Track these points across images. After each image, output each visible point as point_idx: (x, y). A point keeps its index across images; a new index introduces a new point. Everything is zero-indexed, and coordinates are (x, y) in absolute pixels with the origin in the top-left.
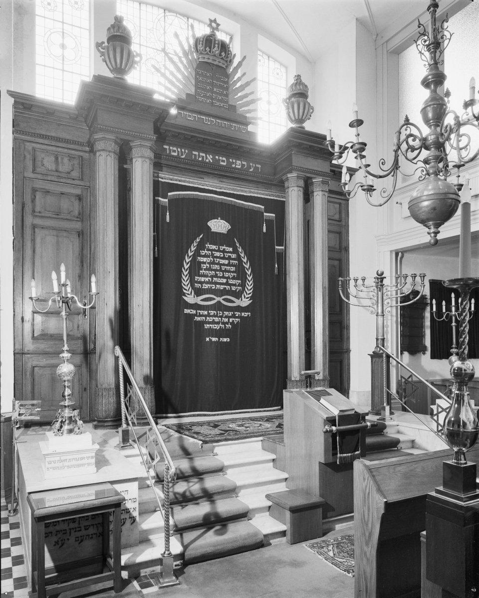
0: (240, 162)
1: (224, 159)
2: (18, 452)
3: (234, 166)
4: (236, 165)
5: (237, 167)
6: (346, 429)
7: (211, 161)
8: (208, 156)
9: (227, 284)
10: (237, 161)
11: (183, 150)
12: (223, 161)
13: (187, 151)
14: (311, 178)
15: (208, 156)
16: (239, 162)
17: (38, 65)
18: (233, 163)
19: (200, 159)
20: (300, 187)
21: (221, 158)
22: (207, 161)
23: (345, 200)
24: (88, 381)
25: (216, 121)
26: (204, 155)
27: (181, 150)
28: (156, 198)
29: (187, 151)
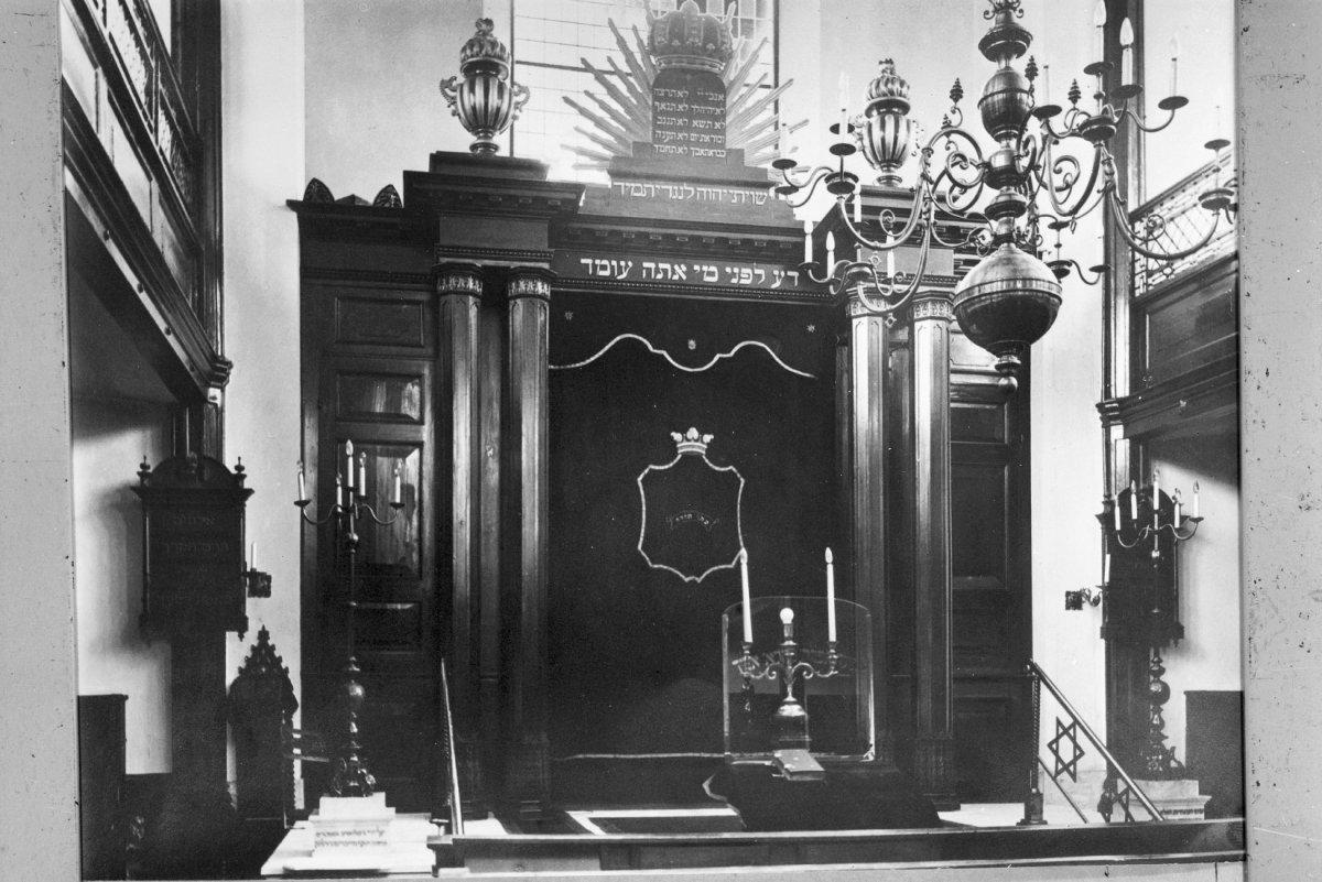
0: (749, 271)
3: (734, 281)
4: (740, 278)
5: (742, 281)
7: (684, 277)
10: (744, 270)
15: (676, 267)
19: (660, 276)
22: (676, 277)
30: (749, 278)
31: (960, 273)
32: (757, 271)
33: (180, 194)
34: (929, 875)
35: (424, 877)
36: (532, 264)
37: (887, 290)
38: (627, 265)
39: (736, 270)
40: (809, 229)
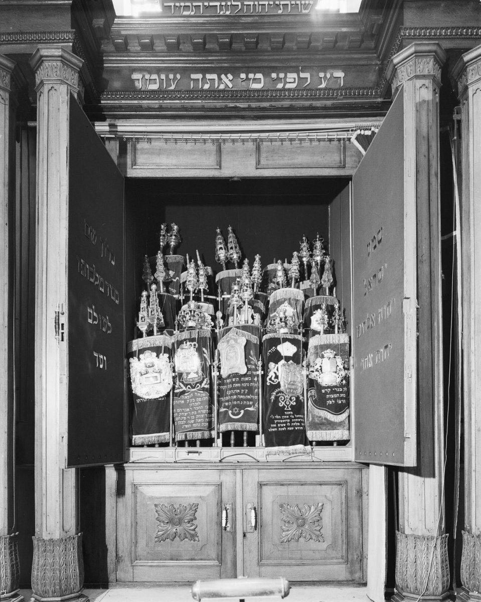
0: (295, 75)
1: (259, 76)
2: (68, 105)
3: (280, 86)
4: (286, 83)
5: (288, 86)
6: (170, 404)
7: (230, 85)
8: (223, 76)
9: (237, 400)
10: (289, 75)
11: (171, 76)
12: (258, 82)
13: (178, 76)
14: (321, 309)
15: (223, 76)
16: (292, 76)
17: (341, 578)
18: (278, 79)
19: (206, 87)
20: (424, 77)
21: (251, 76)
22: (222, 87)
23: (210, 423)
24: (187, 166)
25: (243, 4)
26: (215, 76)
27: (167, 77)
28: (233, 432)
29: (178, 76)
30: (294, 82)
31: (253, 331)
32: (302, 75)
33: (259, 403)
34: (475, 327)
35: (120, 124)
36: (112, 113)
37: (189, 388)
38: (175, 78)
39: (282, 75)
40: (342, 77)
